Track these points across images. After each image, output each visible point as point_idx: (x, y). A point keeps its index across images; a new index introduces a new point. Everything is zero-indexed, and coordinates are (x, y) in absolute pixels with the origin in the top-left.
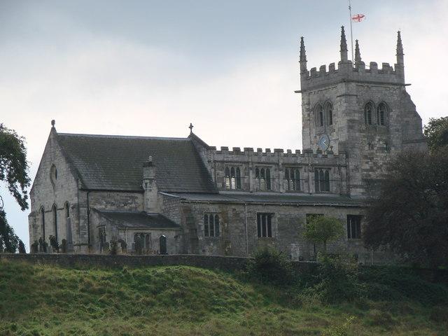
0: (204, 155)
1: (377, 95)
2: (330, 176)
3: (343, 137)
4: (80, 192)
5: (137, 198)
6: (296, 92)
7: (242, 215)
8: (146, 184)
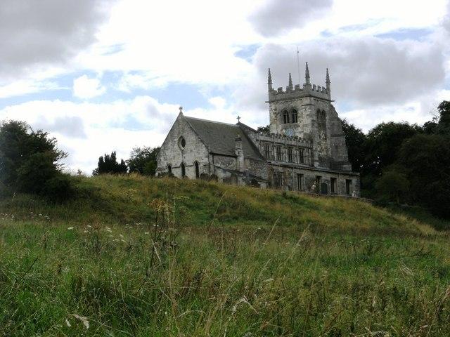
0: (252, 136)
1: (322, 106)
3: (308, 130)
8: (339, 157)
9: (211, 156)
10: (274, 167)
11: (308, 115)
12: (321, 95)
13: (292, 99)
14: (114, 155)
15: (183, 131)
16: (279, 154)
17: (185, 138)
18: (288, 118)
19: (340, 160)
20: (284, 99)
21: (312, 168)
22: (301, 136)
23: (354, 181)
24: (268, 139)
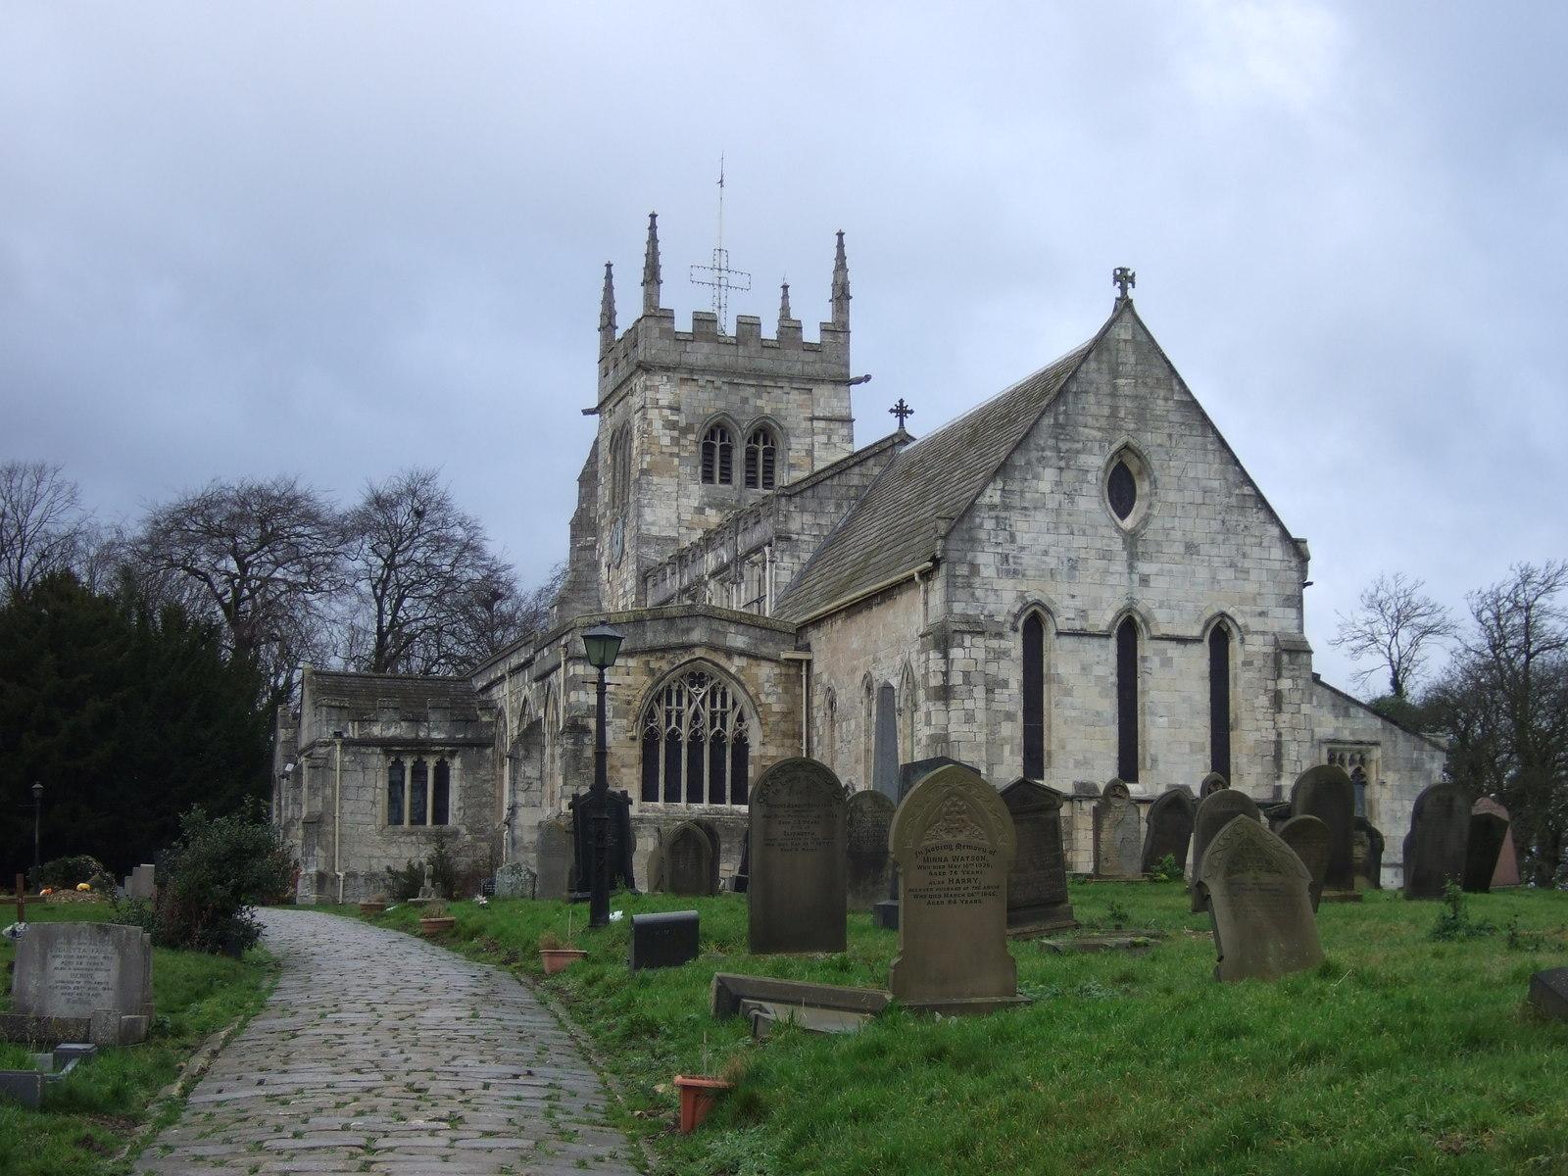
6: (586, 412)
13: (764, 379)
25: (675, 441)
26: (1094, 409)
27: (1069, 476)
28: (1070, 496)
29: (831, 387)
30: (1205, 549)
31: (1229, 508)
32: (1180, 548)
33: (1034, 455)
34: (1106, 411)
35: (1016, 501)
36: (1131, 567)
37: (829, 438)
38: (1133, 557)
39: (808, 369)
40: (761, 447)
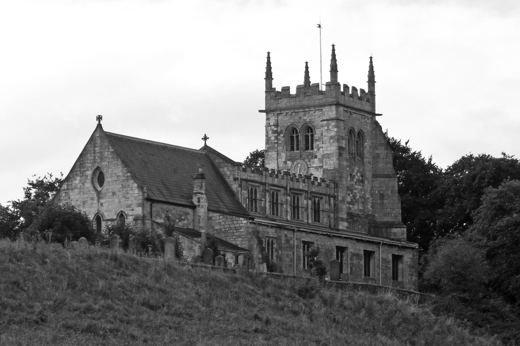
0: (226, 171)
1: (358, 122)
2: (321, 206)
3: (332, 163)
4: (145, 202)
5: (188, 214)
6: (260, 111)
7: (291, 242)
8: (387, 214)
9: (148, 205)
10: (261, 228)
11: (331, 138)
12: (358, 105)
13: (305, 108)
14: (257, 150)
15: (102, 158)
16: (274, 204)
17: (104, 171)
18: (298, 141)
19: (386, 219)
20: (291, 109)
21: (332, 232)
22: (319, 174)
23: (408, 257)
24: (256, 177)
25: (277, 138)
26: (90, 158)
27: (83, 178)
28: (83, 184)
29: (329, 107)
30: (117, 193)
31: (124, 180)
32: (111, 194)
33: (75, 173)
34: (92, 158)
35: (70, 187)
36: (98, 201)
37: (328, 127)
38: (99, 198)
39: (321, 102)
40: (295, 135)
